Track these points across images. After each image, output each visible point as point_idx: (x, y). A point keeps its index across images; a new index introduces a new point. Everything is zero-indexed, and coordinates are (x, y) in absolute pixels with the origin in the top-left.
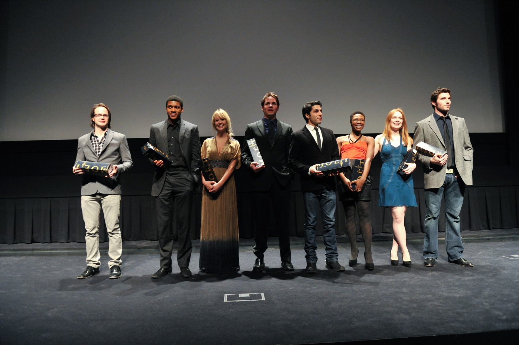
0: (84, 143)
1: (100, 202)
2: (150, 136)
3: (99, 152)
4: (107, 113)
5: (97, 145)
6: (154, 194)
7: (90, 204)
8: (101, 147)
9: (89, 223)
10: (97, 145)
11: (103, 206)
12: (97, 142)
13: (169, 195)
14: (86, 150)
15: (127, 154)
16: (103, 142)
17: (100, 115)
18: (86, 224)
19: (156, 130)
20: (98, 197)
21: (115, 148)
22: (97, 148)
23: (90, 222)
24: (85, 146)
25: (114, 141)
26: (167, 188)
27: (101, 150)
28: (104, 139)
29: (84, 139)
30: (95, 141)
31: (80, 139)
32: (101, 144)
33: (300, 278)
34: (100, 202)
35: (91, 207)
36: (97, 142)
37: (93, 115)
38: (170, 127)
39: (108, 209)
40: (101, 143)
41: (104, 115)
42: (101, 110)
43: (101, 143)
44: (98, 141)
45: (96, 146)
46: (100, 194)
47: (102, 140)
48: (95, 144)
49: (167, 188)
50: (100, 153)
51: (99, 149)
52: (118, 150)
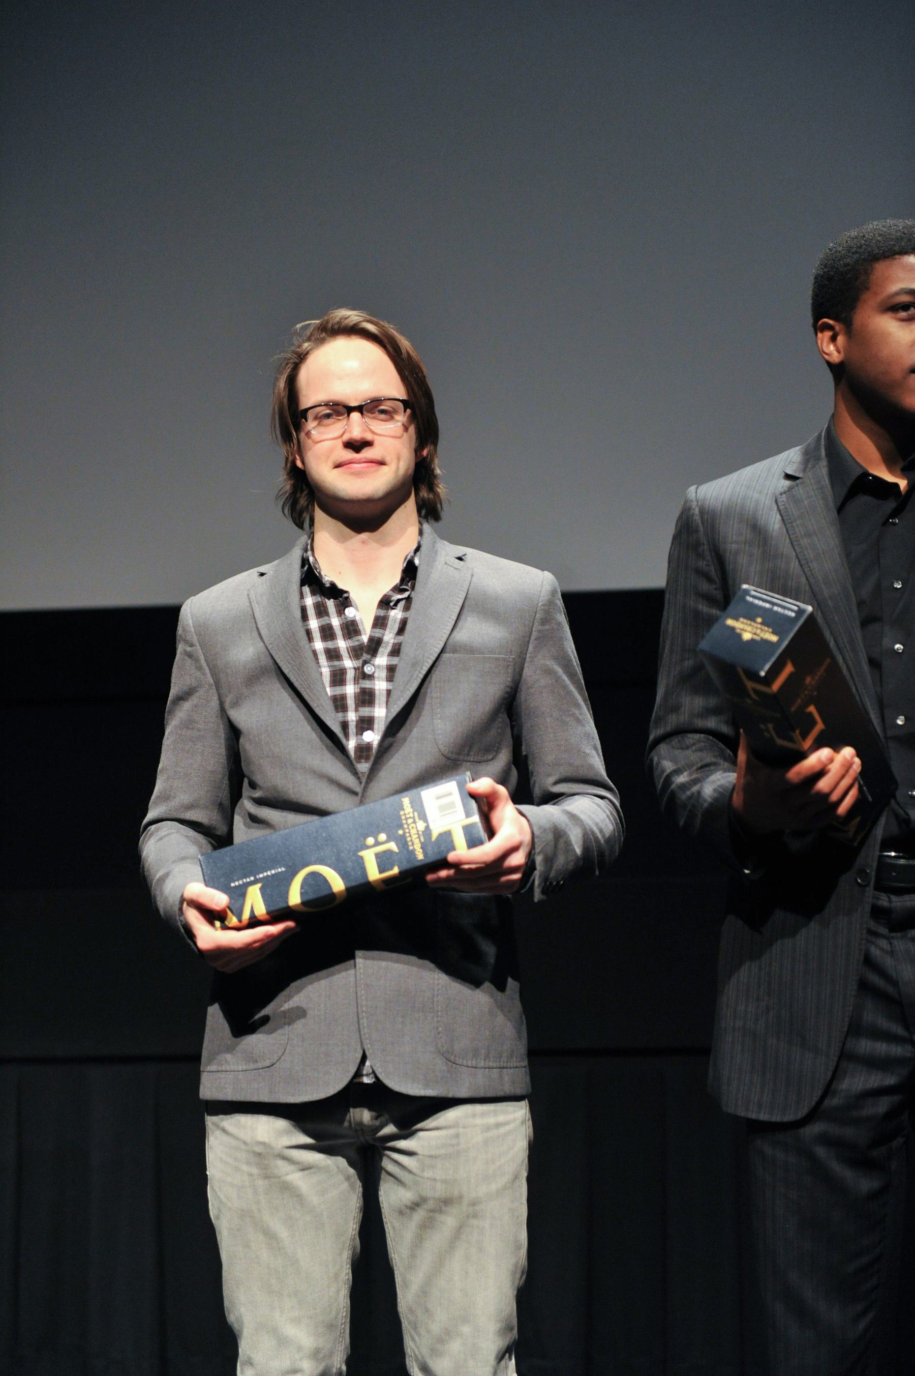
0: (244, 653)
1: (368, 1162)
2: (672, 578)
3: (366, 724)
4: (391, 385)
5: (348, 663)
6: (747, 1087)
7: (295, 1177)
8: (380, 686)
9: (282, 1342)
10: (348, 663)
11: (391, 1196)
12: (342, 644)
13: (882, 1106)
14: (267, 718)
15: (572, 734)
16: (389, 637)
17: (340, 409)
18: (244, 1348)
19: (733, 538)
20: (360, 1123)
21: (492, 691)
22: (350, 690)
23: (291, 1331)
24: (254, 677)
25: (478, 632)
26: (882, 1048)
27: (381, 713)
28: (396, 614)
29: (229, 608)
30: (327, 633)
31: (201, 608)
32: (382, 660)
33: (355, 1202)
34: (368, 1162)
35: (299, 1197)
36: (342, 644)
37: (292, 418)
38: (863, 500)
39: (449, 1221)
40: (374, 646)
41: (372, 407)
42: (346, 368)
43: (374, 646)
44: (351, 629)
45: (338, 678)
46: (377, 1096)
47: (380, 622)
48: (333, 655)
49: (882, 1048)
50: (372, 737)
51: (366, 698)
52: (511, 707)
